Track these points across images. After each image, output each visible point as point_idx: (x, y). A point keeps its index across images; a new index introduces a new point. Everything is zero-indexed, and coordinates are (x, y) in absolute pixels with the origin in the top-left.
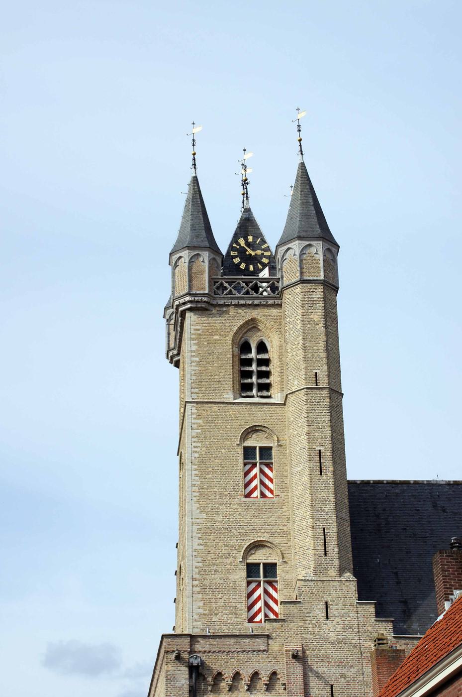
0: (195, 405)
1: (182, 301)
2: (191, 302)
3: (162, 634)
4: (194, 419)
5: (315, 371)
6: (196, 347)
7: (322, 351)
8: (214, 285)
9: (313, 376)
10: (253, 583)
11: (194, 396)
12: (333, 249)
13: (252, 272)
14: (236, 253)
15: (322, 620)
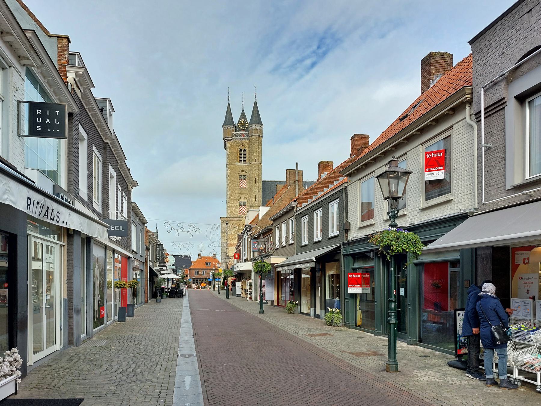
11: (228, 163)
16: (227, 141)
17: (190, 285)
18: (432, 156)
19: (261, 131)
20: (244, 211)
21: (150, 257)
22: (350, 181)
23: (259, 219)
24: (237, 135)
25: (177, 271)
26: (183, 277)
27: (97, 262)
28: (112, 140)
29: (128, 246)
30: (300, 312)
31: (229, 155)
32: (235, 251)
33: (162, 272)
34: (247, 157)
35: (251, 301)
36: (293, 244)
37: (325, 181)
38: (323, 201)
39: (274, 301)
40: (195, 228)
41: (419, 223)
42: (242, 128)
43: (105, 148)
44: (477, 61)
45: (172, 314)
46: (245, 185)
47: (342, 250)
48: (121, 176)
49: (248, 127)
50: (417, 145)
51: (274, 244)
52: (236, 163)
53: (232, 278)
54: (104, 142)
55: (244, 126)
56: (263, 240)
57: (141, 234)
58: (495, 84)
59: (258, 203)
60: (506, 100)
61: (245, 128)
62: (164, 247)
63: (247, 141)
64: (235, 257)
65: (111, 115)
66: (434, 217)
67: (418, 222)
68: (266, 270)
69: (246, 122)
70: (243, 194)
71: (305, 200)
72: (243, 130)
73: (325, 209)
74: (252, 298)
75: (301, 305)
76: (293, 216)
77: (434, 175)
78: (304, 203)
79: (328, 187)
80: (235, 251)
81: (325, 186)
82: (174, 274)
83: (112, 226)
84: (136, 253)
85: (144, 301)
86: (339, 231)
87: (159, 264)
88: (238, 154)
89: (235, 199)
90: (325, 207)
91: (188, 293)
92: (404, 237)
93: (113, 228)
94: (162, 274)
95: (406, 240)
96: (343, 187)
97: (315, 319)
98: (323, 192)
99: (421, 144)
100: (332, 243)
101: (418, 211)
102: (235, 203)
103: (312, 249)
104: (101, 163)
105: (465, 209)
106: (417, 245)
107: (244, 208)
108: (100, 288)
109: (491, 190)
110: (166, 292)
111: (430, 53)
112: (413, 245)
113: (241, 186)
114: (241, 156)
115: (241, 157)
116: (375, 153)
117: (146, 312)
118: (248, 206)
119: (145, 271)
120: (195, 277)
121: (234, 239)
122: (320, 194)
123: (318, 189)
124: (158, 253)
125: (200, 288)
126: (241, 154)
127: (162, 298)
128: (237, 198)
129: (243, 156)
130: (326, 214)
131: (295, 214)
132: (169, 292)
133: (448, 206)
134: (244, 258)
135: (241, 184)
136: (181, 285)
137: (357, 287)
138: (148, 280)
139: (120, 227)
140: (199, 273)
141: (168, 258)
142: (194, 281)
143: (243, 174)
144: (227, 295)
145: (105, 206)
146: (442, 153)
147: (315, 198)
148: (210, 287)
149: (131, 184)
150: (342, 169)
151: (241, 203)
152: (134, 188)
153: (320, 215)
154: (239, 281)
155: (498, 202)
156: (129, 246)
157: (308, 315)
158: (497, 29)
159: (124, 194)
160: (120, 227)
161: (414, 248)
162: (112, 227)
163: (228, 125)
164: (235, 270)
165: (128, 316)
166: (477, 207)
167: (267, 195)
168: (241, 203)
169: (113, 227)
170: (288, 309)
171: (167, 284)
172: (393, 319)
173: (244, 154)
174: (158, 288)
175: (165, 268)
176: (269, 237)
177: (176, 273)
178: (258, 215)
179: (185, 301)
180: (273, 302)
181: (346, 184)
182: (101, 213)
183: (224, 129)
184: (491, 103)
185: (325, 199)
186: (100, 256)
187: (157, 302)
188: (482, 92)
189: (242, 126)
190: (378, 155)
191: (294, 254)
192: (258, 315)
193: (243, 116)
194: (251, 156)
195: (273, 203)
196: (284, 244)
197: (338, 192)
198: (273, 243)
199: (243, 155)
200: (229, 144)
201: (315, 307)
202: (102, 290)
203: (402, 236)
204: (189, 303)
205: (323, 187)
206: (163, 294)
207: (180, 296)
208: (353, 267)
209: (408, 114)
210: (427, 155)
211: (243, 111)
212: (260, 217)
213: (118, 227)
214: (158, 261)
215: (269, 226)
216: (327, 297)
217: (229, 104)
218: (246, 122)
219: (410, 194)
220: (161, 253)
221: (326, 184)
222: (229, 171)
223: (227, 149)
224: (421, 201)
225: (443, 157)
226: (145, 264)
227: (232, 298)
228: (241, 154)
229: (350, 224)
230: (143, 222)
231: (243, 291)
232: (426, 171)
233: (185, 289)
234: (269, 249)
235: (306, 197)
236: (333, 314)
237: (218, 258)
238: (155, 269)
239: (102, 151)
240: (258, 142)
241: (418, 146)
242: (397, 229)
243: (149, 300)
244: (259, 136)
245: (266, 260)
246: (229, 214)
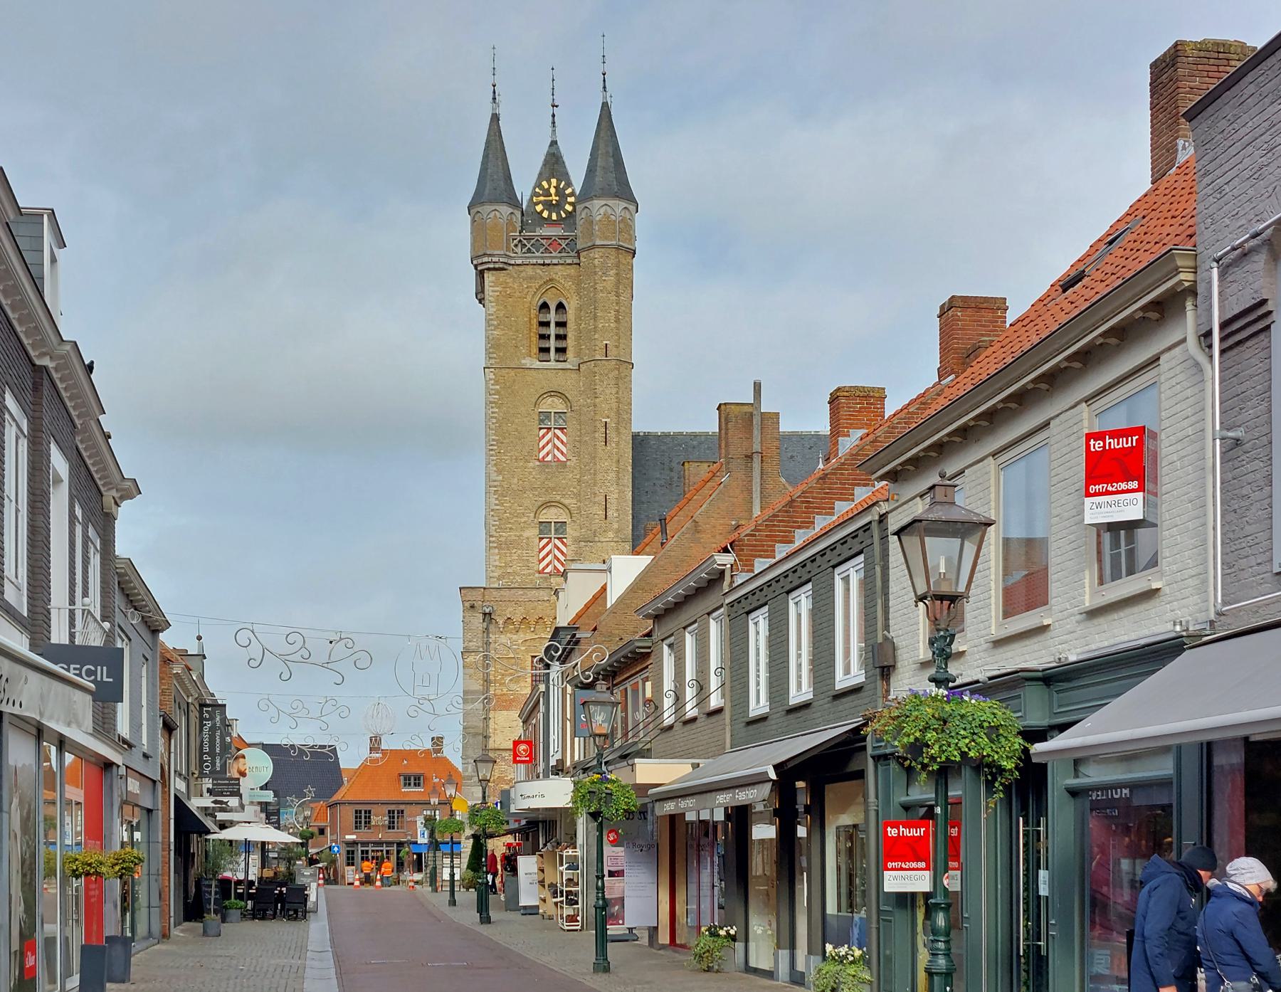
0: (493, 370)
4: (492, 385)
5: (605, 342)
9: (603, 347)
11: (493, 361)
16: (489, 269)
17: (336, 871)
18: (1107, 448)
19: (627, 227)
20: (558, 560)
21: (178, 762)
22: (896, 497)
23: (609, 605)
24: (529, 246)
25: (278, 810)
26: (306, 838)
27: (16, 785)
28: (62, 357)
29: (104, 723)
30: (742, 966)
31: (496, 327)
32: (518, 731)
33: (221, 816)
34: (570, 335)
35: (576, 930)
36: (719, 711)
37: (842, 474)
38: (815, 560)
39: (656, 928)
40: (351, 651)
41: (1082, 657)
42: (550, 215)
43: (36, 388)
44: (1205, 175)
45: (269, 976)
46: (562, 453)
47: (869, 738)
48: (83, 469)
49: (574, 210)
50: (1073, 403)
51: (656, 708)
52: (523, 361)
53: (509, 839)
54: (34, 365)
55: (558, 206)
56: (606, 696)
57: (144, 674)
58: (1245, 255)
59: (616, 526)
60: (1269, 306)
61: (564, 215)
62: (229, 714)
63: (572, 271)
64: (515, 755)
65: (54, 260)
66: (1118, 640)
67: (1078, 654)
68: (617, 810)
69: (564, 189)
70: (553, 489)
71: (763, 546)
72: (555, 223)
73: (821, 588)
74: (579, 918)
75: (747, 941)
76: (721, 606)
77: (1113, 506)
78: (761, 556)
79: (853, 495)
80: (518, 731)
81: (841, 494)
82: (269, 823)
83: (72, 666)
84: (130, 746)
85: (156, 928)
86: (864, 671)
87: (210, 786)
88: (535, 322)
89: (520, 510)
90: (823, 580)
91: (327, 902)
92: (962, 716)
93: (78, 672)
94: (223, 826)
95: (968, 726)
96: (872, 515)
97: (788, 989)
98: (833, 514)
99: (994, 455)
100: (844, 714)
101: (1079, 617)
102: (522, 529)
103: (785, 733)
104: (26, 441)
105: (1188, 622)
106: (1003, 740)
107: (558, 549)
108: (24, 875)
109: (1243, 570)
110: (239, 897)
111: (1176, 45)
112: (992, 741)
113: (543, 458)
114: (543, 331)
115: (544, 337)
116: (984, 398)
117: (172, 967)
118: (577, 540)
119: (160, 812)
120: (354, 837)
121: (517, 680)
122: (821, 522)
123: (813, 503)
124: (206, 741)
125: (378, 883)
126: (547, 324)
127: (224, 920)
128: (526, 509)
129: (553, 330)
130: (824, 608)
131: (727, 601)
132: (251, 897)
133: (1032, 644)
134: (553, 762)
135: (543, 447)
136: (299, 870)
137: (913, 869)
138: (172, 847)
139: (99, 668)
140: (374, 820)
141: (244, 757)
142: (353, 852)
143: (555, 405)
144: (483, 907)
145: (38, 590)
146: (1135, 438)
147: (801, 537)
148: (418, 877)
149: (114, 493)
150: (905, 428)
151: (544, 527)
152: (126, 504)
153: (763, 626)
154: (534, 850)
155: (1259, 607)
156: (109, 723)
157: (770, 974)
158: (1248, 92)
159: (91, 532)
160: (99, 668)
161: (992, 747)
162: (71, 669)
163: (491, 202)
164: (513, 810)
165: (111, 980)
166: (1212, 616)
167: (654, 492)
168: (544, 527)
169: (75, 669)
170: (700, 956)
171: (243, 865)
172: (940, 961)
173: (559, 324)
174: (211, 879)
175: (233, 802)
176: (639, 679)
177: (278, 822)
178: (604, 589)
179: (317, 929)
180: (654, 931)
181: (884, 508)
182: (26, 615)
183: (473, 221)
184: (1236, 311)
185: (822, 553)
186: (24, 765)
187: (205, 933)
188: (1215, 272)
189: (549, 205)
190: (969, 420)
191: (724, 748)
192: (588, 978)
193: (554, 164)
194: (590, 331)
195: (662, 544)
196: (691, 710)
197: (861, 531)
198: (654, 705)
199: (553, 325)
200: (496, 284)
201: (793, 946)
202: (28, 881)
203: (956, 713)
204: (332, 940)
205: (831, 498)
206: (227, 903)
207: (296, 912)
208: (904, 799)
209: (1084, 271)
210: (1092, 442)
211: (554, 143)
212: (612, 598)
213: (93, 669)
214: (207, 771)
215: (637, 640)
216: (831, 908)
217: (495, 118)
218: (568, 191)
219: (1059, 560)
220: (218, 741)
221: (845, 484)
222: (497, 392)
223: (486, 302)
224: (1087, 585)
225: (1137, 451)
226: (159, 786)
227: (499, 921)
228: (547, 324)
229: (894, 649)
230: (154, 625)
231: (546, 893)
232: (1088, 495)
233: (314, 885)
234: (641, 726)
235: (767, 536)
236: (840, 967)
237: (453, 753)
238: (196, 804)
239: (29, 398)
240: (617, 274)
241: (1078, 407)
242: (946, 693)
243: (175, 927)
244: (618, 248)
245: (618, 774)
246: (496, 574)
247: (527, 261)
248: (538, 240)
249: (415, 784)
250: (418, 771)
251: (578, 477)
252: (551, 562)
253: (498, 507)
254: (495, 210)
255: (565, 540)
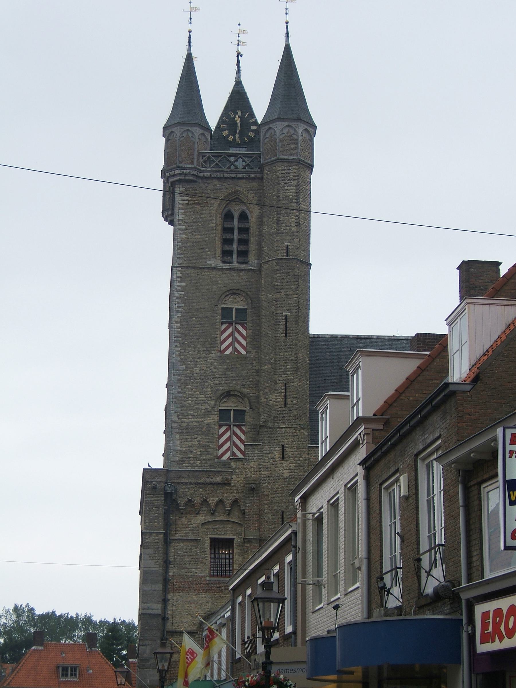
0: (180, 269)
1: (172, 173)
2: (180, 174)
3: (143, 468)
5: (286, 244)
6: (184, 216)
7: (294, 225)
8: (202, 159)
10: (224, 426)
12: (310, 129)
13: (239, 144)
14: (225, 126)
15: (278, 460)
24: (217, 161)
34: (252, 240)
52: (209, 262)
61: (247, 140)
151: (224, 415)
247: (214, 175)
248: (225, 157)
249: (71, 675)
250: (75, 663)
251: (257, 368)
252: (229, 437)
253: (181, 395)
254: (188, 130)
255: (243, 428)
